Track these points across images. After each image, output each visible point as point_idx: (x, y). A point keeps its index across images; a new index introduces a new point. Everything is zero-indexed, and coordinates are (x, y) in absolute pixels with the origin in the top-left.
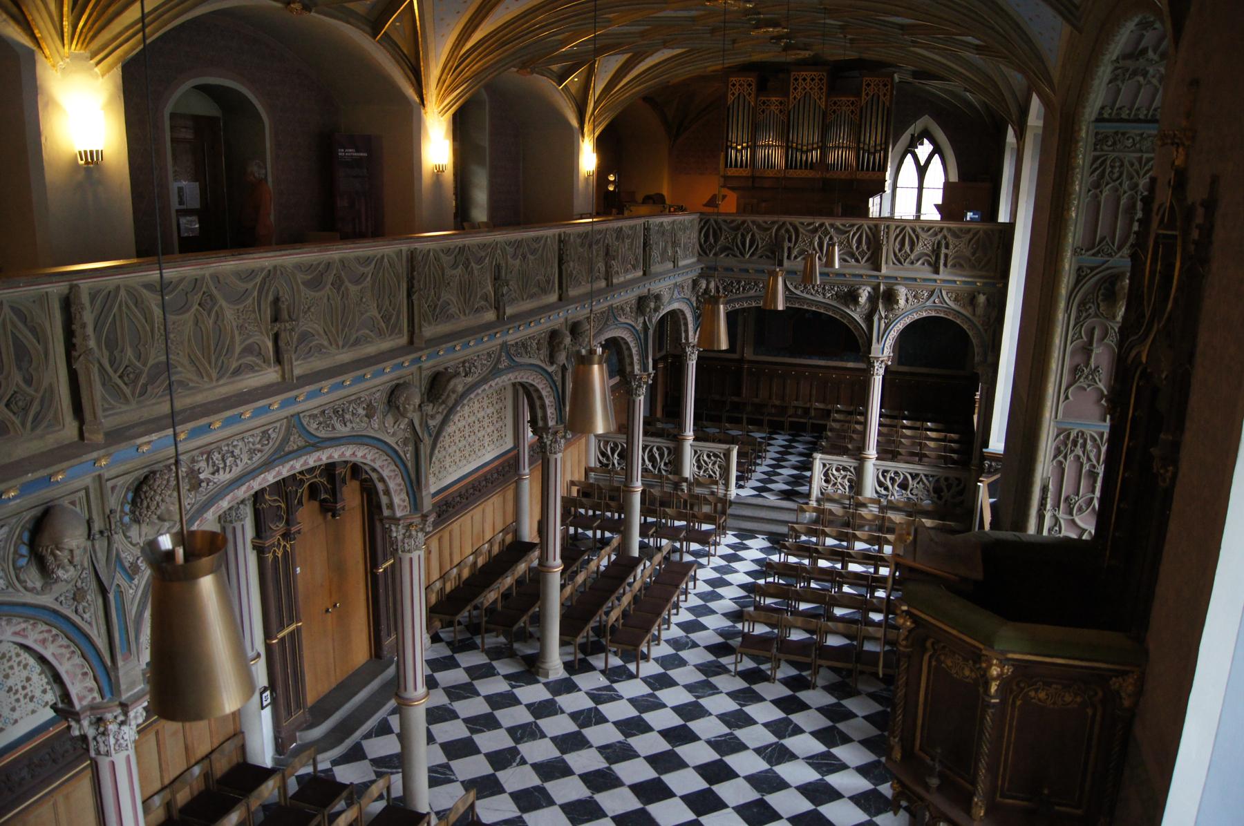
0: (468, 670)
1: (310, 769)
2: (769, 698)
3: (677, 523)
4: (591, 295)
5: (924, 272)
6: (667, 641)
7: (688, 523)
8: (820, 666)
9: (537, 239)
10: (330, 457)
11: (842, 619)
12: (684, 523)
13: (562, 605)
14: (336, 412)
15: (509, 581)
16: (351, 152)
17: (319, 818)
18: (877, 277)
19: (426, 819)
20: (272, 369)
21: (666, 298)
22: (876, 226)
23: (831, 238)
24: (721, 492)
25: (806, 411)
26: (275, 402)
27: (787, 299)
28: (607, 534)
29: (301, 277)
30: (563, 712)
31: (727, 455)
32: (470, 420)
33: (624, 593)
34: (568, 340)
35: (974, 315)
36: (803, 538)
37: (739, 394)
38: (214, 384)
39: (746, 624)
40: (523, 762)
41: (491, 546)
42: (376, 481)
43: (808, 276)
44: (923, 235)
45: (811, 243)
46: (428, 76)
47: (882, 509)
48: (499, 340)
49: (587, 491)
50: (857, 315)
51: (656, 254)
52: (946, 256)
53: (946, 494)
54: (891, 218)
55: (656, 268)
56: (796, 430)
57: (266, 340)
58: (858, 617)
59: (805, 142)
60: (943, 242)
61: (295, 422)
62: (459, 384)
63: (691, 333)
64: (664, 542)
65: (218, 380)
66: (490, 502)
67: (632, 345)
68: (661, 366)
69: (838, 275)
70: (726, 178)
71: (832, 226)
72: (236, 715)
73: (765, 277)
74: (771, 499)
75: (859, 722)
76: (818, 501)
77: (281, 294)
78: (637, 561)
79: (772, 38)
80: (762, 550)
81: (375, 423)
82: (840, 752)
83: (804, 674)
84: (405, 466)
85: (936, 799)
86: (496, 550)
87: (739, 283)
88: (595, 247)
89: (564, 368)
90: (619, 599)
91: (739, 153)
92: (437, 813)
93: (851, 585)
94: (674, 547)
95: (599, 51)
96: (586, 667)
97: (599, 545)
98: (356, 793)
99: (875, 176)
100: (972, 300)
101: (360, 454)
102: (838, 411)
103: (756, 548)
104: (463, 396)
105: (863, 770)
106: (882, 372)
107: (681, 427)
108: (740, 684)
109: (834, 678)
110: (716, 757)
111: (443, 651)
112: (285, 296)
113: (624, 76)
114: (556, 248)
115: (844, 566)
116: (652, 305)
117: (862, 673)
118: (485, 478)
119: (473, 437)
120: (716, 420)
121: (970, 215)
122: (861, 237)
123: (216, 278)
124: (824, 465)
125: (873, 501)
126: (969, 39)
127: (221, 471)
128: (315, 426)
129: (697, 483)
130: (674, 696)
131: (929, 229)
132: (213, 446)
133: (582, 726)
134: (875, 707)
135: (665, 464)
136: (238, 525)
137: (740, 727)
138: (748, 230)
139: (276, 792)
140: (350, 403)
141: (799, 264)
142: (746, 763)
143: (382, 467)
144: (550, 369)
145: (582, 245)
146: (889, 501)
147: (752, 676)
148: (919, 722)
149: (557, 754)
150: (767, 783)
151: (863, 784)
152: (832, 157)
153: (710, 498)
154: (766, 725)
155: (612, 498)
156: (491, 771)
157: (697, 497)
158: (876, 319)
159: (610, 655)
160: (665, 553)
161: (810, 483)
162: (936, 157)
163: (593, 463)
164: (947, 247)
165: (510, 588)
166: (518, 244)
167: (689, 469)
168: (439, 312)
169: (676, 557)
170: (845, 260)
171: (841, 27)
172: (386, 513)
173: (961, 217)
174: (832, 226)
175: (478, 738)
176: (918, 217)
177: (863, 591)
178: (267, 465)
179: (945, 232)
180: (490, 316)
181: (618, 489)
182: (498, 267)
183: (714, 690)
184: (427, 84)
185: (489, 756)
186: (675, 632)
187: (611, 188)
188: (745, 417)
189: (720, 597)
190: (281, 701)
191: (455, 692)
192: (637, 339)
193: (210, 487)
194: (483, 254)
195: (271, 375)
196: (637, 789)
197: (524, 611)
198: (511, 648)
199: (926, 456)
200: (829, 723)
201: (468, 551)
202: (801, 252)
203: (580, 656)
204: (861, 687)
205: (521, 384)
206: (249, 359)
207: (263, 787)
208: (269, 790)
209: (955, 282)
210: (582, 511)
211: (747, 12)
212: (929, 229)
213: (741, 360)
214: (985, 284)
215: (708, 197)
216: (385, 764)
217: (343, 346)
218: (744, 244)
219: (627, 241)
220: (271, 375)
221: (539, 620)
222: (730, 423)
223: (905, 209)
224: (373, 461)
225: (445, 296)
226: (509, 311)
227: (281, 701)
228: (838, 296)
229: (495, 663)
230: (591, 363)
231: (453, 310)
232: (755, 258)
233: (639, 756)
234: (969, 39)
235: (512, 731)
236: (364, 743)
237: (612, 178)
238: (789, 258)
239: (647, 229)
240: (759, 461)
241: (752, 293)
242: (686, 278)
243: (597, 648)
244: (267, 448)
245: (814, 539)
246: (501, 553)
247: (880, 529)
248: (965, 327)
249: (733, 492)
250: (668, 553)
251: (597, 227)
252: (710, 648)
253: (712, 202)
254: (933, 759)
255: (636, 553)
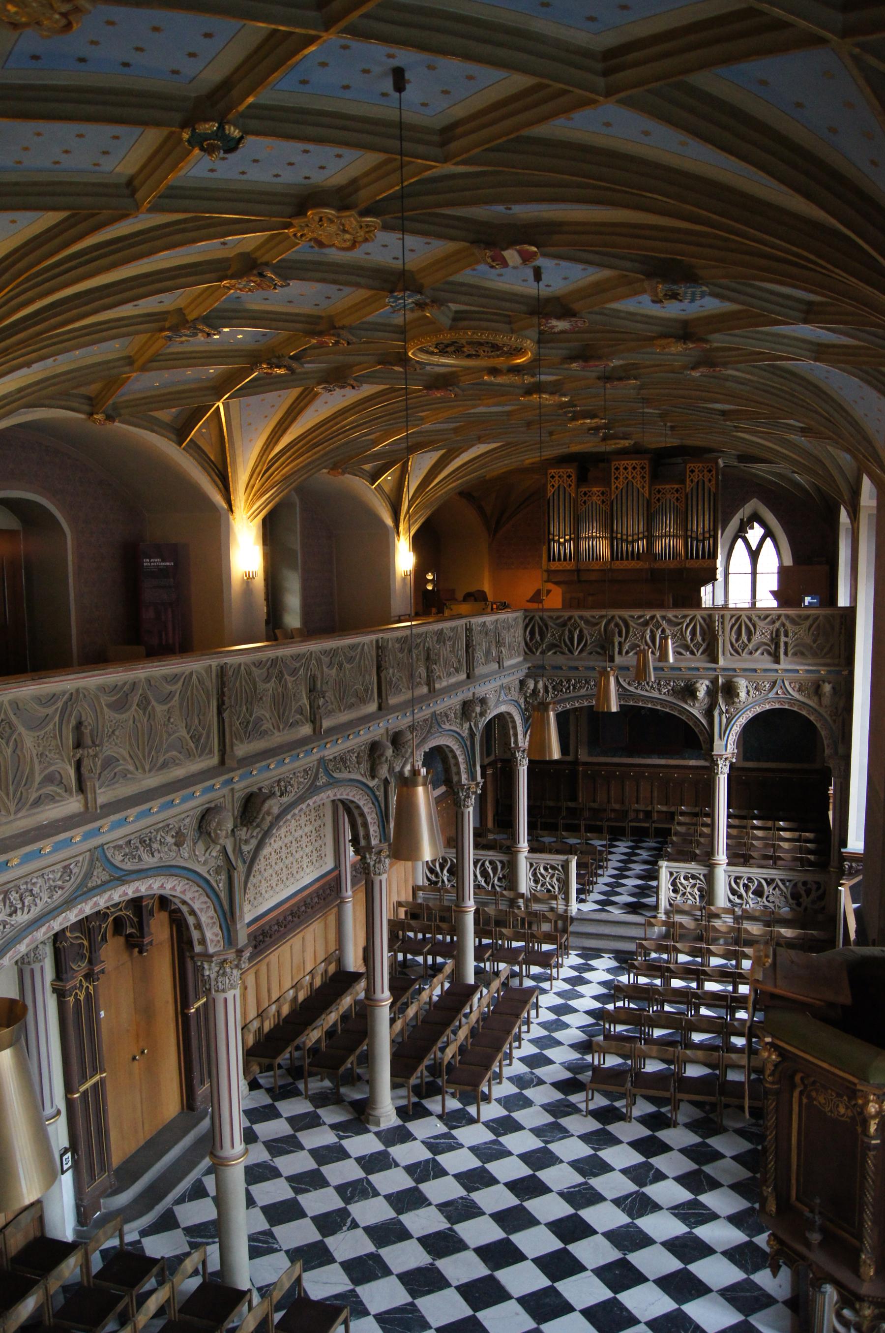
0: (291, 1120)
1: (115, 1242)
2: (626, 1139)
3: (515, 944)
4: (412, 703)
5: (763, 661)
6: (510, 1079)
7: (527, 943)
8: (680, 1101)
9: (353, 647)
10: (137, 890)
11: (700, 1046)
12: (523, 944)
13: (393, 1042)
14: (143, 841)
15: (332, 1017)
16: (157, 562)
17: (126, 1300)
18: (715, 669)
19: (248, 1297)
20: (75, 798)
21: (491, 702)
22: (710, 616)
23: (663, 631)
24: (561, 908)
25: (648, 814)
26: (77, 834)
27: (620, 696)
28: (439, 960)
29: (104, 699)
30: (397, 1165)
31: (566, 867)
32: (287, 840)
33: (460, 1027)
34: (389, 752)
35: (820, 705)
36: (654, 955)
37: (574, 798)
38: (12, 817)
39: (596, 1056)
40: (355, 1225)
41: (313, 978)
42: (187, 915)
43: (641, 673)
44: (761, 624)
45: (643, 636)
46: (236, 482)
47: (737, 919)
48: (316, 755)
49: (415, 913)
50: (696, 711)
51: (479, 655)
52: (786, 644)
53: (805, 901)
54: (725, 607)
55: (480, 670)
56: (639, 836)
57: (69, 767)
58: (719, 1042)
59: (630, 532)
60: (782, 630)
61: (98, 856)
62: (274, 806)
63: (520, 737)
64: (502, 966)
65: (16, 812)
66: (311, 928)
67: (458, 753)
68: (489, 772)
69: (673, 669)
70: (548, 571)
71: (663, 618)
72: (38, 1203)
73: (595, 674)
74: (616, 913)
75: (727, 1163)
76: (667, 913)
77: (83, 719)
78: (473, 989)
79: (590, 429)
80: (608, 971)
81: (185, 852)
82: (709, 1199)
83: (663, 1110)
84: (217, 896)
85: (819, 1258)
86: (318, 982)
87: (569, 681)
88: (415, 652)
89: (386, 782)
90: (455, 1033)
91: (562, 545)
92: (259, 1289)
93: (708, 1006)
94: (512, 971)
95: (412, 449)
96: (421, 1112)
97: (430, 972)
98: (168, 1268)
99: (706, 563)
100: (817, 690)
101: (168, 886)
102: (682, 814)
103: (602, 969)
104: (279, 817)
105: (735, 1220)
106: (726, 770)
107: (514, 838)
108: (593, 1125)
109: (697, 1114)
110: (570, 1211)
111: (262, 1099)
112: (89, 720)
113: (439, 473)
114: (374, 653)
115: (700, 986)
116: (478, 709)
117: (727, 1106)
118: (305, 903)
119: (291, 859)
120: (551, 828)
121: (808, 600)
122: (695, 626)
123: (15, 704)
124: (671, 874)
125: (726, 911)
126: (792, 422)
127: (19, 912)
128: (120, 858)
129: (535, 898)
130: (521, 1142)
131: (766, 617)
132: (12, 884)
133: (419, 1181)
134: (745, 1146)
135: (499, 879)
136: (36, 967)
137: (595, 1175)
138: (575, 626)
139: (78, 1270)
140: (157, 831)
141: (631, 659)
142: (605, 1217)
143: (193, 899)
144: (372, 784)
145: (401, 650)
146: (744, 911)
147: (606, 1115)
148: (794, 1167)
149: (392, 1214)
150: (629, 1239)
151: (735, 1236)
152: (659, 546)
153: (549, 915)
154: (624, 1171)
155: (442, 919)
156: (318, 1237)
157: (535, 914)
158: (716, 713)
159: (447, 1097)
160: (503, 978)
161: (657, 893)
162: (768, 541)
163: (421, 881)
164: (786, 635)
165: (335, 1024)
166: (334, 653)
167: (525, 884)
168: (252, 729)
169: (515, 983)
170: (680, 654)
171: (660, 416)
172: (198, 949)
173: (798, 603)
174: (663, 618)
175: (303, 1199)
176: (754, 604)
177: (722, 1012)
178: (69, 903)
179: (783, 619)
180: (306, 730)
181: (449, 909)
182: (313, 678)
183: (565, 1133)
184: (235, 490)
185: (316, 1220)
186: (519, 1068)
187: (430, 587)
188: (582, 823)
189: (567, 1026)
190: (84, 1164)
191: (277, 1147)
192: (463, 746)
193: (7, 930)
194: (298, 665)
195: (73, 805)
196: (484, 1252)
197: (352, 1050)
198: (338, 1092)
199: (780, 858)
200: (695, 1167)
201: (288, 984)
202: (634, 647)
203: (415, 1099)
204: (726, 1122)
205: (341, 801)
206: (50, 789)
207: (63, 1266)
208: (70, 1269)
209: (797, 671)
210: (411, 934)
211: (562, 405)
212: (766, 617)
213: (576, 762)
214: (829, 672)
215: (530, 594)
216: (201, 1233)
217: (150, 771)
218: (571, 640)
219: (448, 643)
220: (73, 805)
221: (368, 1059)
222: (566, 831)
223: (739, 597)
224: (184, 892)
225: (258, 712)
226: (326, 724)
227: (84, 1164)
228: (675, 692)
229: (320, 1111)
230: (415, 785)
231: (266, 726)
232: (584, 654)
233: (484, 1214)
234: (792, 422)
235: (341, 1189)
236: (176, 1208)
237: (430, 577)
238: (620, 653)
239: (469, 629)
240: (600, 872)
241: (583, 692)
242: (512, 679)
243: (432, 1090)
244: (68, 885)
245: (665, 956)
246: (323, 985)
247: (737, 942)
248: (812, 718)
249: (574, 907)
250: (507, 978)
251: (415, 631)
252: (558, 1085)
253: (537, 598)
254: (812, 1211)
255: (471, 980)
